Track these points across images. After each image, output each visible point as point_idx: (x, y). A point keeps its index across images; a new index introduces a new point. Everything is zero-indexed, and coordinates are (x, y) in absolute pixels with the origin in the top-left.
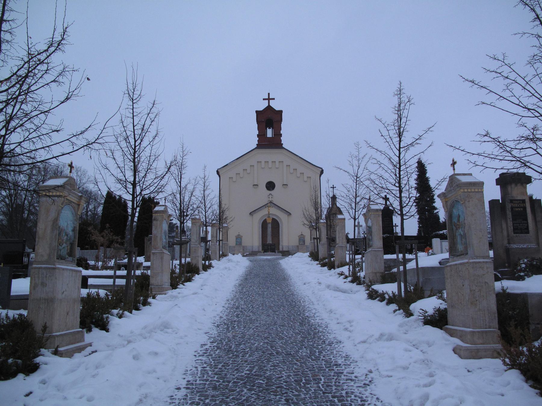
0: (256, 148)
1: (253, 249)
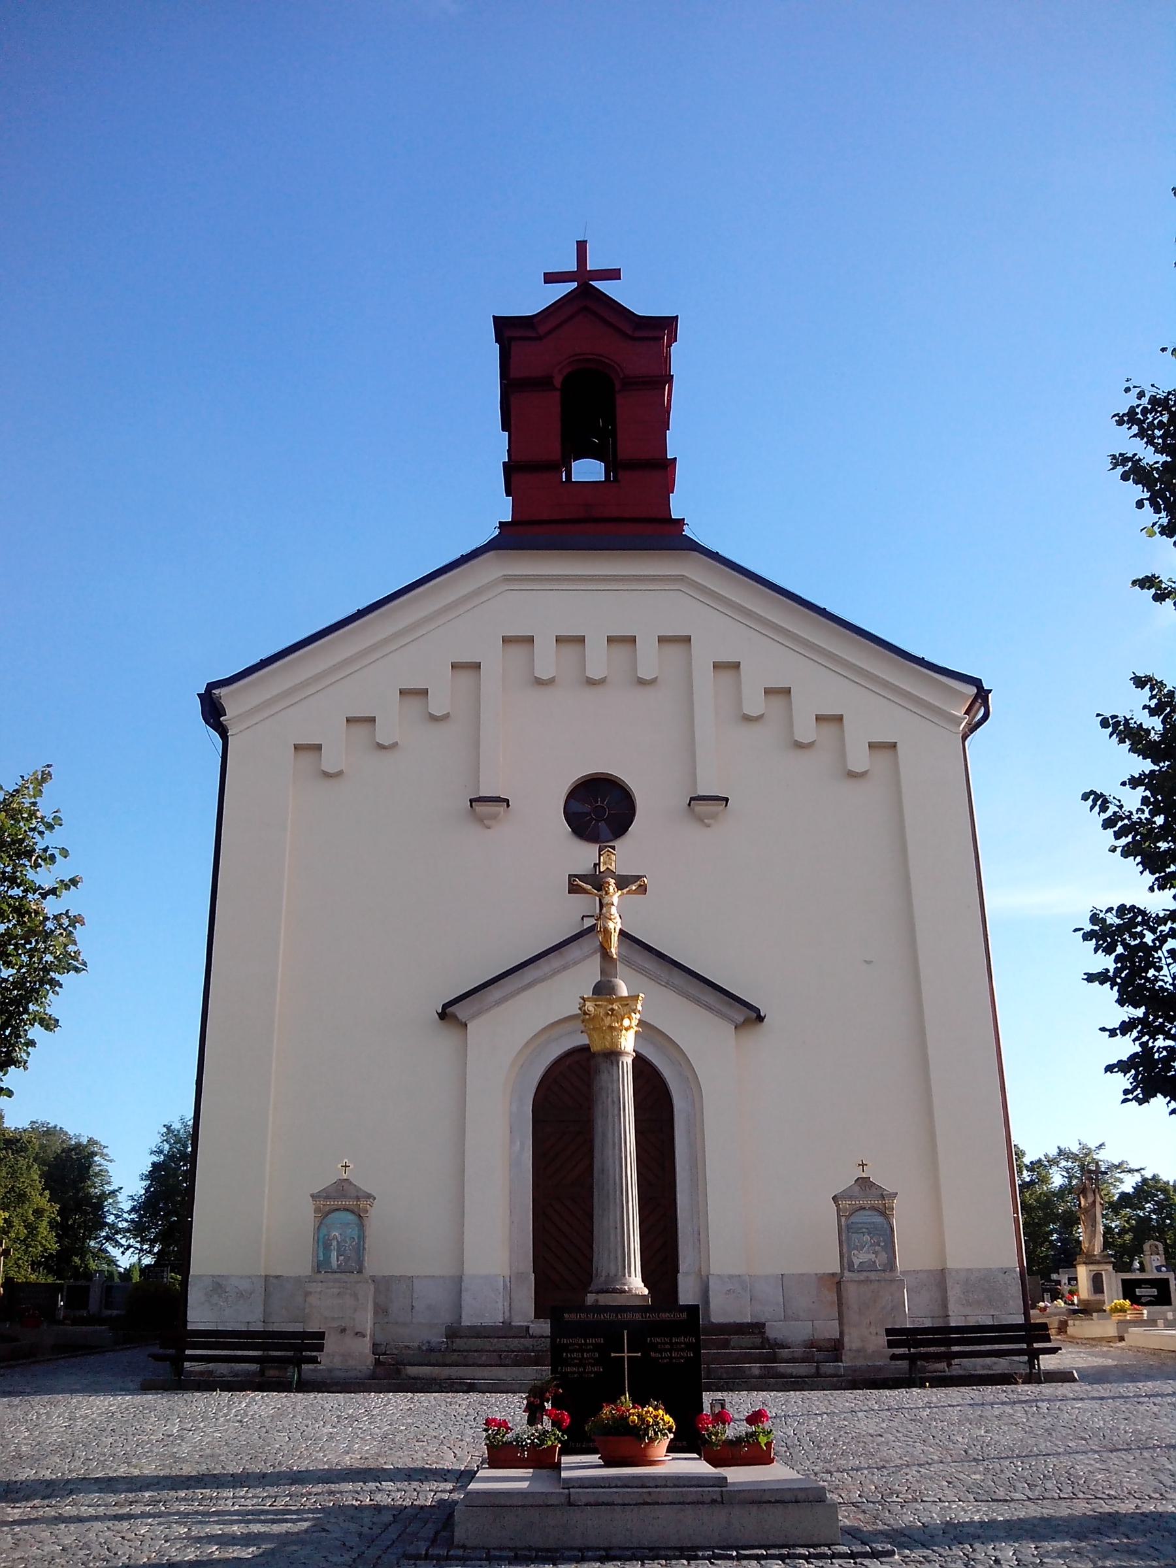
0: (491, 546)
1: (459, 1306)
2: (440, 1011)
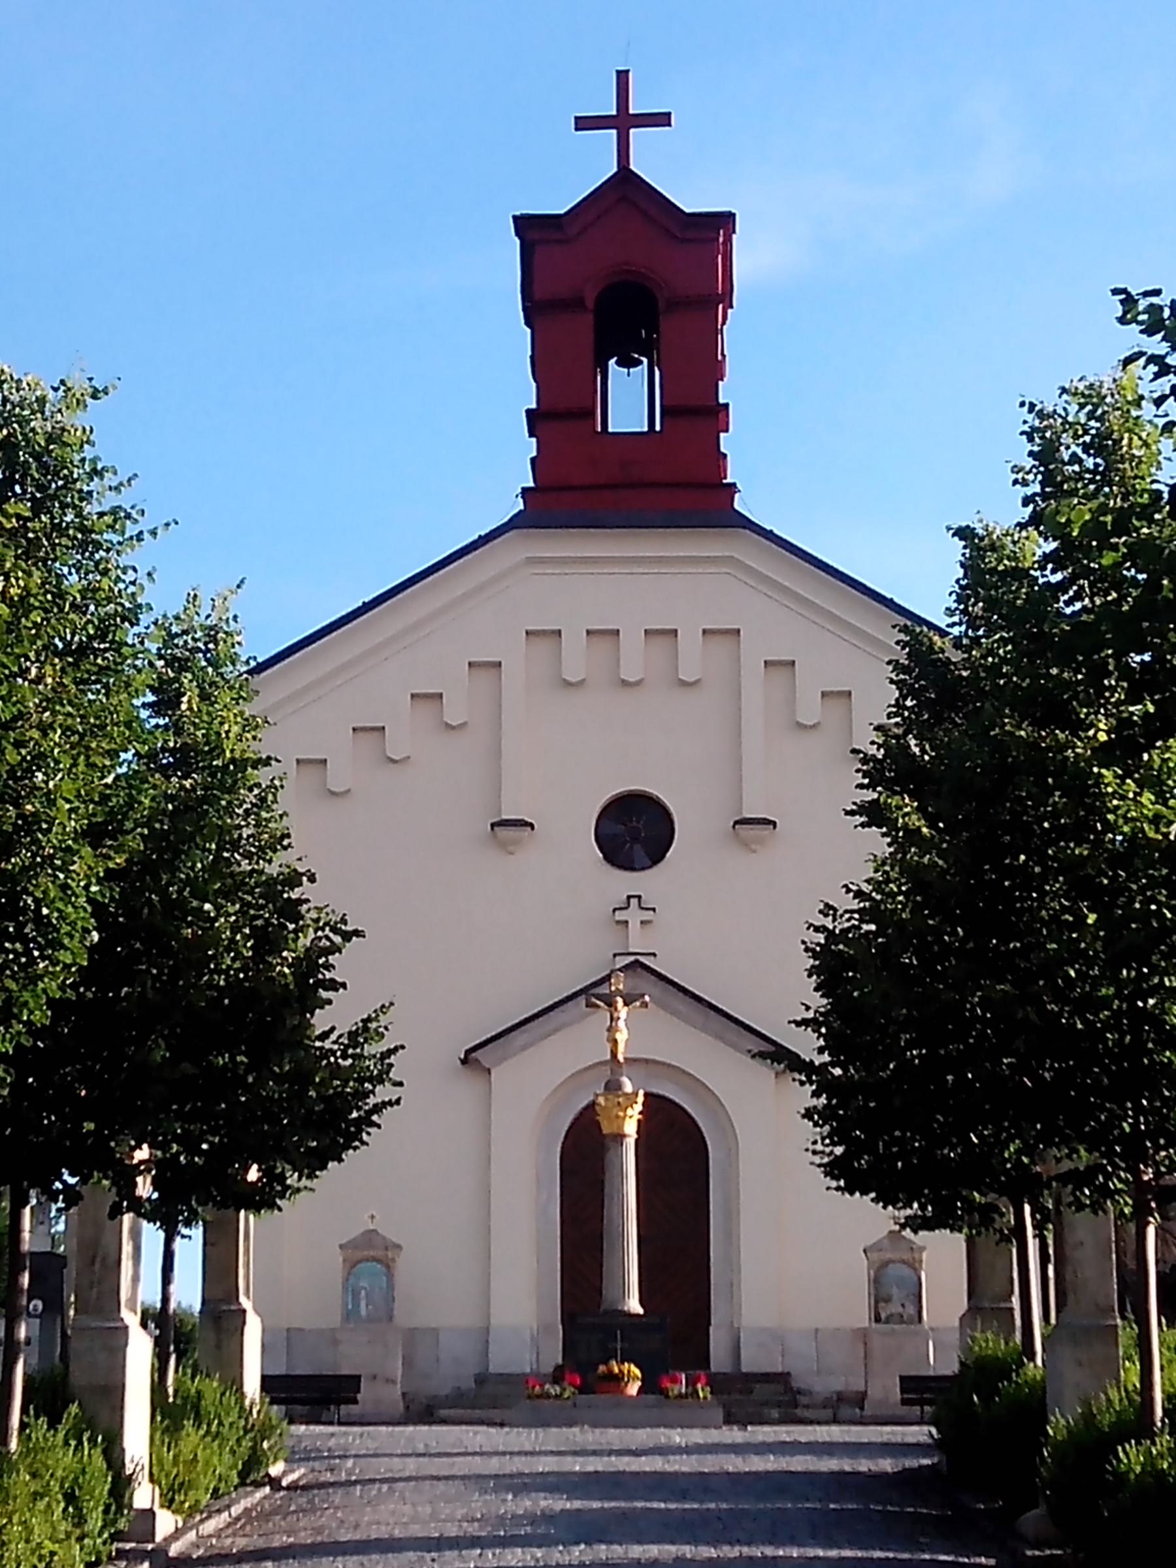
2: (462, 1056)
